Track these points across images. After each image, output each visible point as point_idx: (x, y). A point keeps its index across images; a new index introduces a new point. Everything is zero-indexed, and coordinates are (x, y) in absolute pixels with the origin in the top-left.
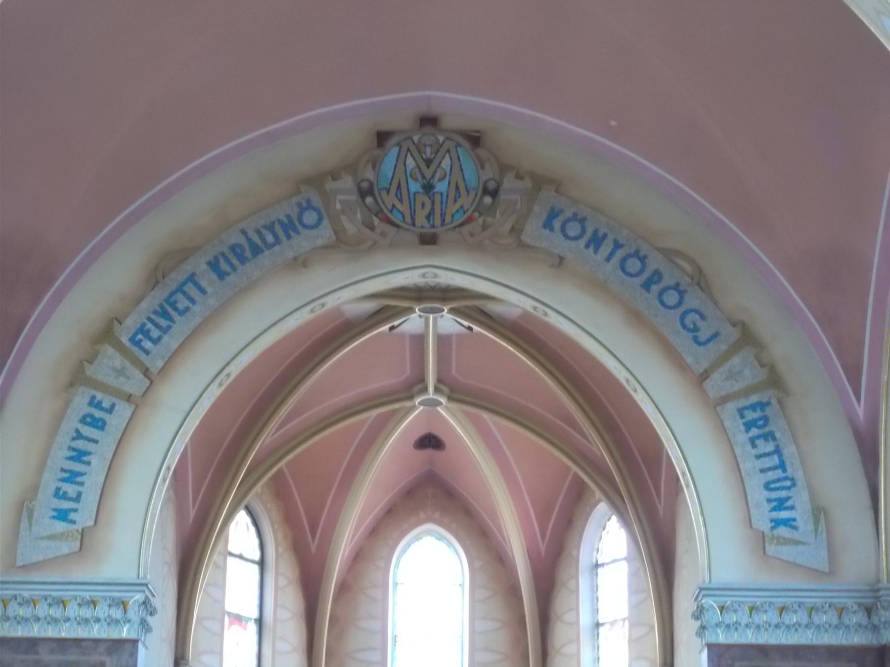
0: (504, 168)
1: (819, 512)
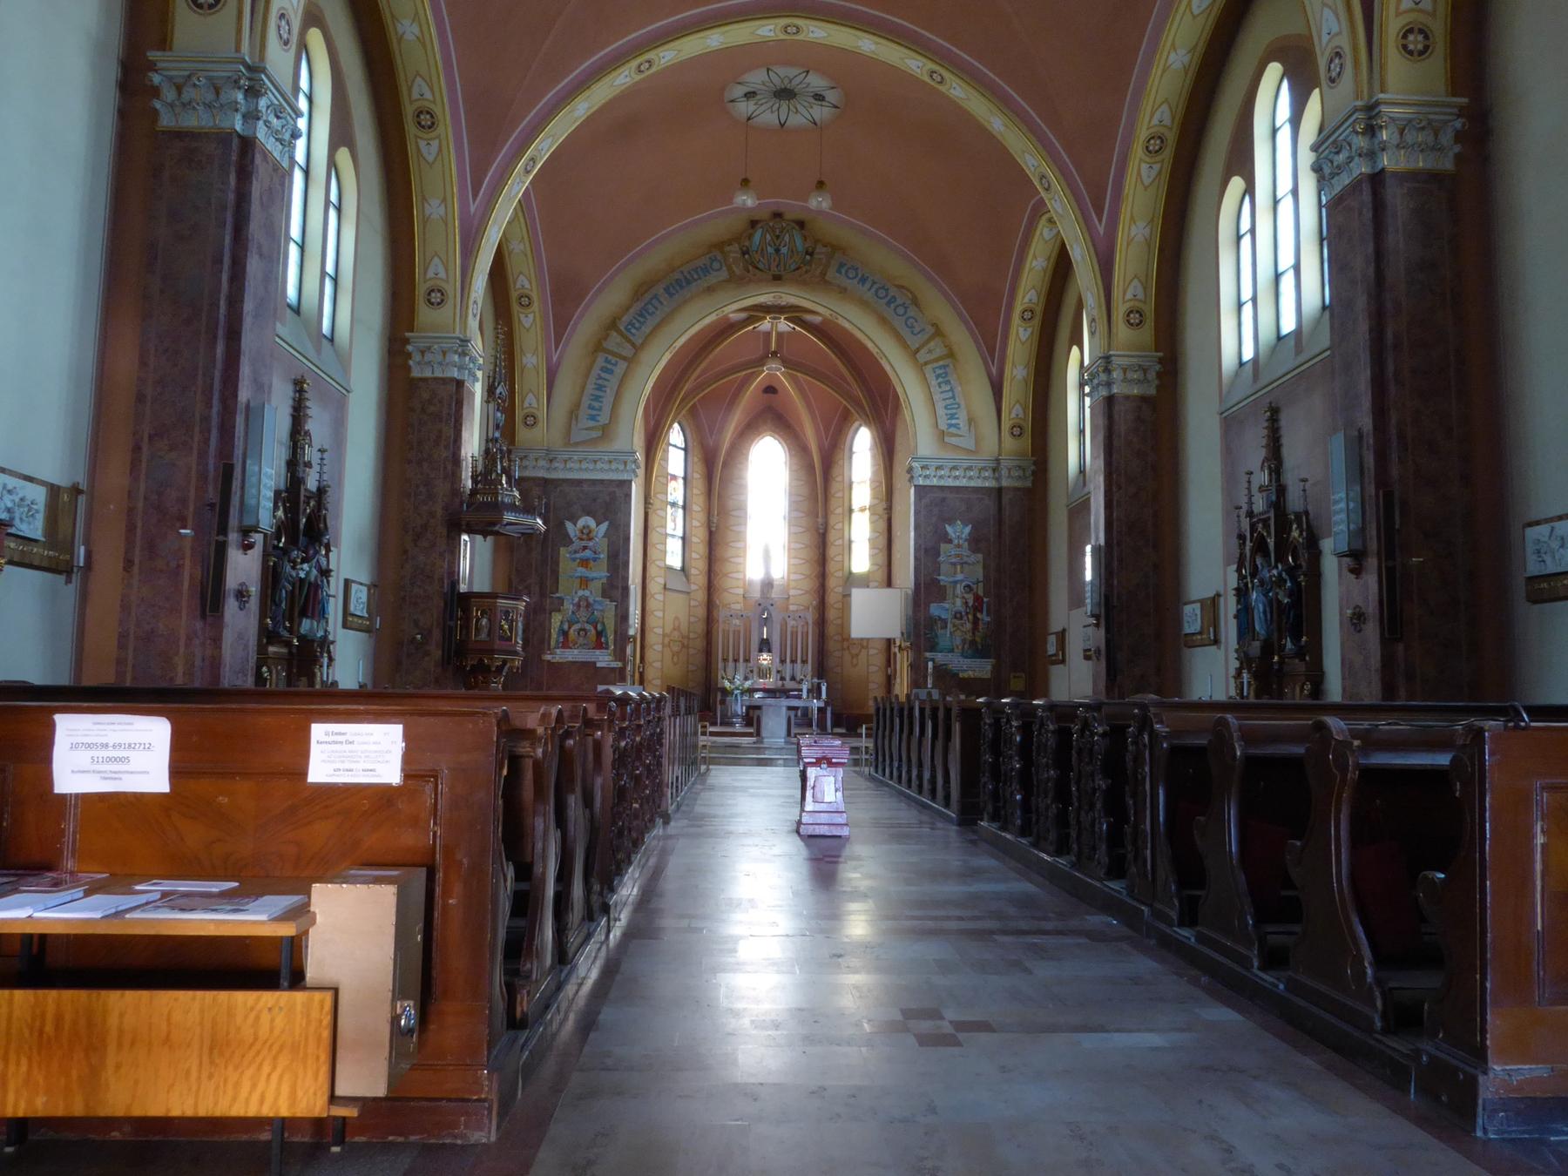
0: (817, 241)
1: (971, 421)
